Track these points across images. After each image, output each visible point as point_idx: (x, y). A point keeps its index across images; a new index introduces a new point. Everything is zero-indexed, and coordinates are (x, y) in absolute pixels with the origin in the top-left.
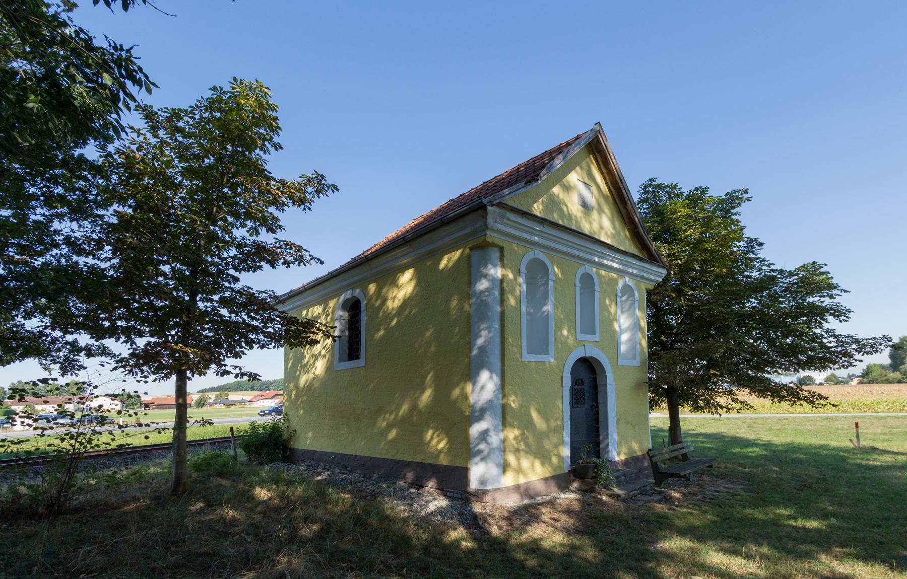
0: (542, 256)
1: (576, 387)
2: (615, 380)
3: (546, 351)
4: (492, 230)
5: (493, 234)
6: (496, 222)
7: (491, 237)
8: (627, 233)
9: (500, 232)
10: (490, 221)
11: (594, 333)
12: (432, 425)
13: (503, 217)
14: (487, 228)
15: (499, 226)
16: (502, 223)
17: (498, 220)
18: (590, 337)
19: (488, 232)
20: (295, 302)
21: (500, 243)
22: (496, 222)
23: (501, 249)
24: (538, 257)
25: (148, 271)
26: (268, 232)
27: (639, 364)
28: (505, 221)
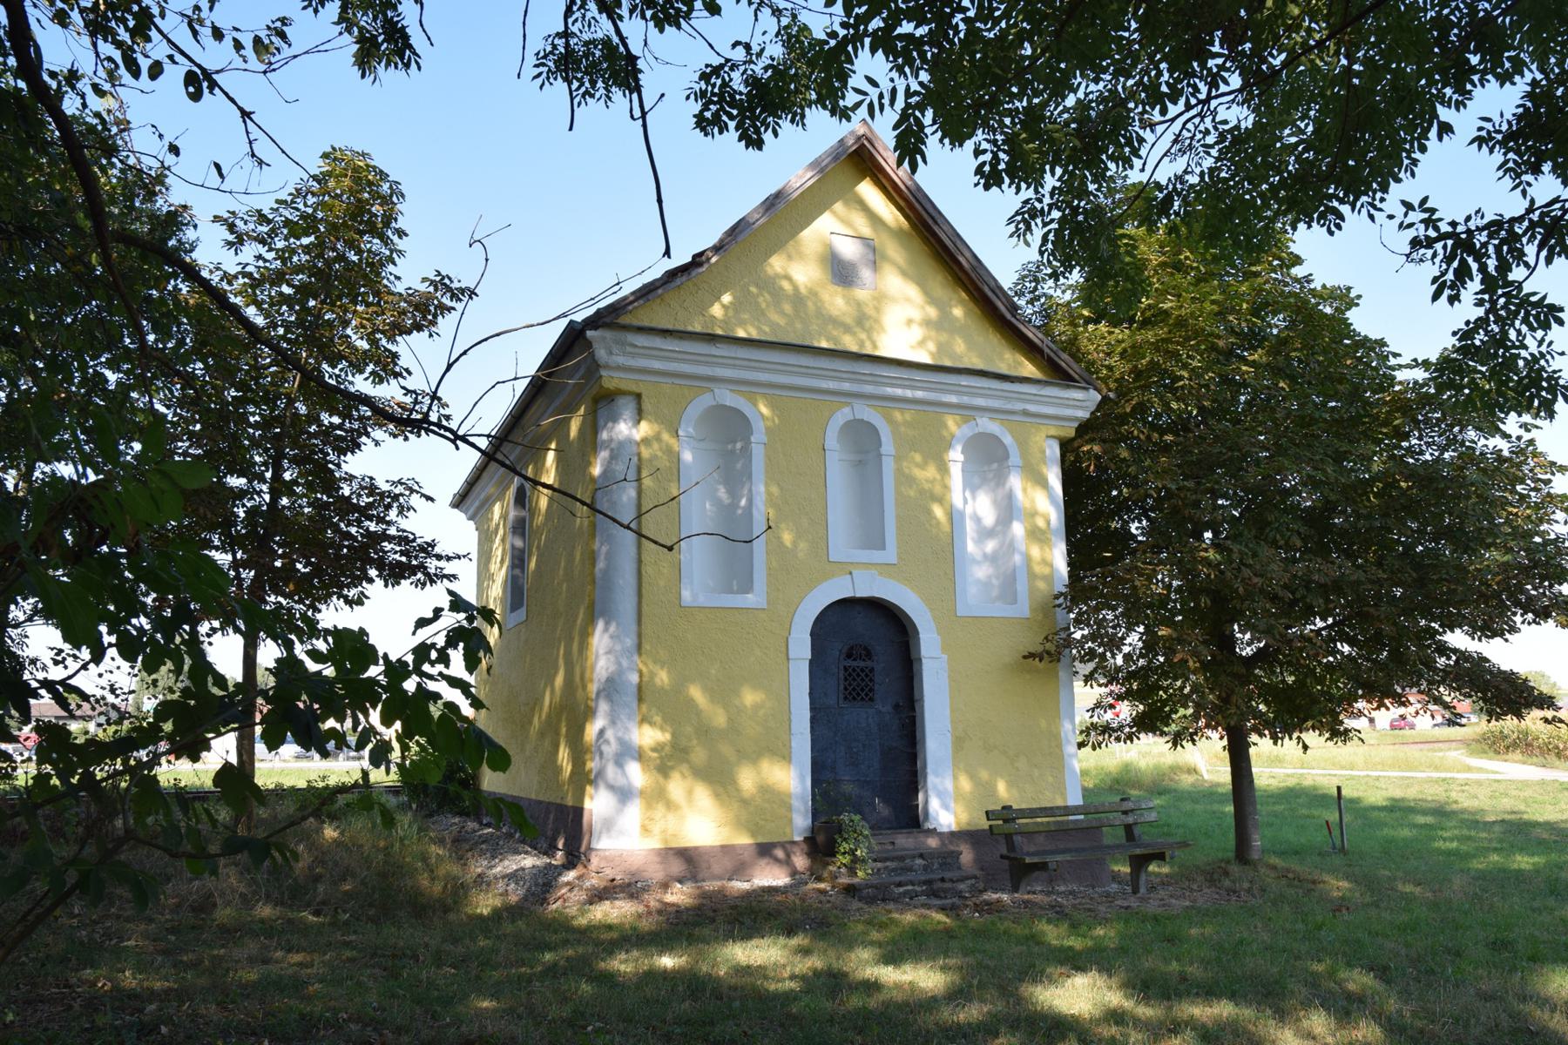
0: (729, 398)
1: (850, 663)
2: (946, 648)
3: (747, 587)
4: (607, 367)
5: (612, 374)
6: (611, 353)
7: (611, 380)
8: (963, 294)
9: (619, 368)
10: (601, 354)
11: (884, 548)
12: (933, 842)
13: (623, 344)
14: (598, 366)
15: (620, 360)
16: (625, 354)
17: (615, 351)
18: (876, 556)
19: (603, 373)
20: (479, 494)
21: (635, 389)
22: (611, 353)
23: (638, 396)
24: (721, 402)
25: (12, 1022)
26: (662, 31)
27: (1026, 613)
28: (629, 349)
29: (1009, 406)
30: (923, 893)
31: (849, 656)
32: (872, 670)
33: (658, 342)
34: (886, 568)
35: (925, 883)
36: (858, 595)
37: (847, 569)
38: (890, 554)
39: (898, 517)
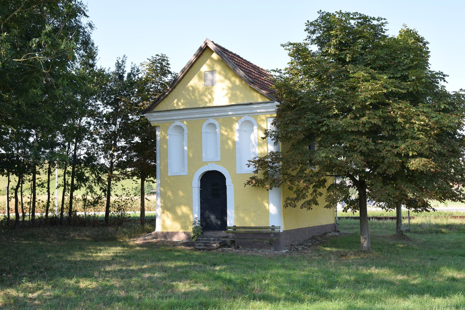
0: (178, 123)
16: (153, 118)
29: (251, 112)
30: (203, 246)
31: (213, 186)
32: (218, 189)
33: (158, 114)
34: (217, 162)
35: (204, 243)
36: (210, 170)
37: (206, 163)
38: (219, 159)
39: (221, 148)
